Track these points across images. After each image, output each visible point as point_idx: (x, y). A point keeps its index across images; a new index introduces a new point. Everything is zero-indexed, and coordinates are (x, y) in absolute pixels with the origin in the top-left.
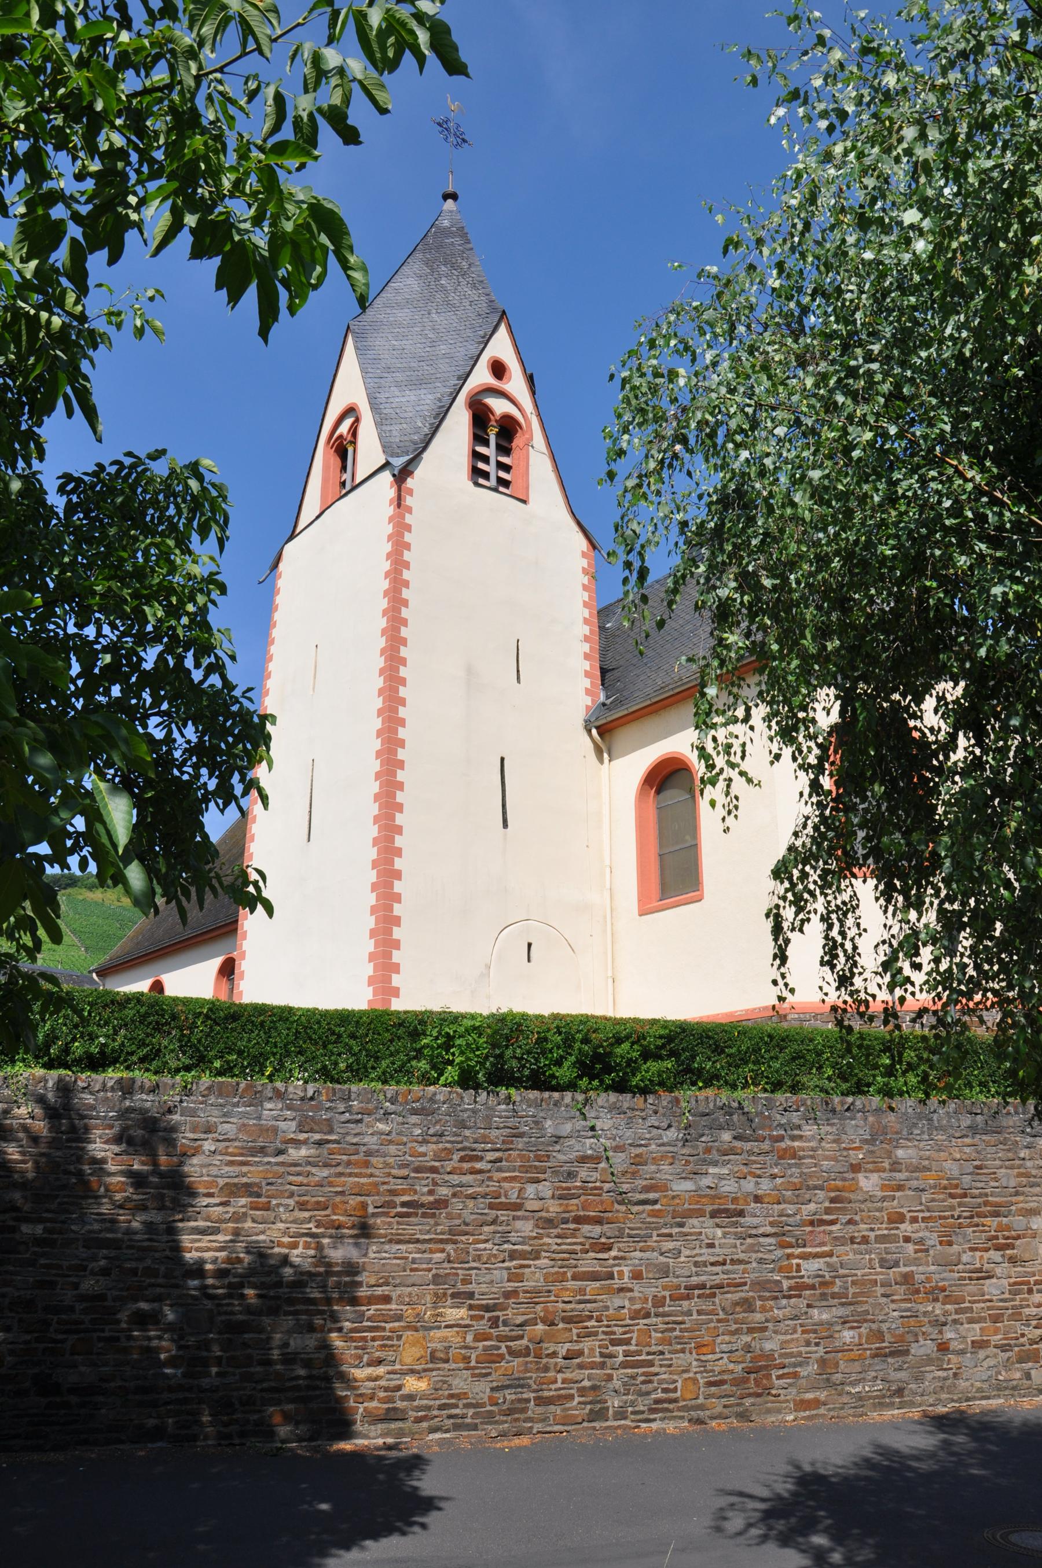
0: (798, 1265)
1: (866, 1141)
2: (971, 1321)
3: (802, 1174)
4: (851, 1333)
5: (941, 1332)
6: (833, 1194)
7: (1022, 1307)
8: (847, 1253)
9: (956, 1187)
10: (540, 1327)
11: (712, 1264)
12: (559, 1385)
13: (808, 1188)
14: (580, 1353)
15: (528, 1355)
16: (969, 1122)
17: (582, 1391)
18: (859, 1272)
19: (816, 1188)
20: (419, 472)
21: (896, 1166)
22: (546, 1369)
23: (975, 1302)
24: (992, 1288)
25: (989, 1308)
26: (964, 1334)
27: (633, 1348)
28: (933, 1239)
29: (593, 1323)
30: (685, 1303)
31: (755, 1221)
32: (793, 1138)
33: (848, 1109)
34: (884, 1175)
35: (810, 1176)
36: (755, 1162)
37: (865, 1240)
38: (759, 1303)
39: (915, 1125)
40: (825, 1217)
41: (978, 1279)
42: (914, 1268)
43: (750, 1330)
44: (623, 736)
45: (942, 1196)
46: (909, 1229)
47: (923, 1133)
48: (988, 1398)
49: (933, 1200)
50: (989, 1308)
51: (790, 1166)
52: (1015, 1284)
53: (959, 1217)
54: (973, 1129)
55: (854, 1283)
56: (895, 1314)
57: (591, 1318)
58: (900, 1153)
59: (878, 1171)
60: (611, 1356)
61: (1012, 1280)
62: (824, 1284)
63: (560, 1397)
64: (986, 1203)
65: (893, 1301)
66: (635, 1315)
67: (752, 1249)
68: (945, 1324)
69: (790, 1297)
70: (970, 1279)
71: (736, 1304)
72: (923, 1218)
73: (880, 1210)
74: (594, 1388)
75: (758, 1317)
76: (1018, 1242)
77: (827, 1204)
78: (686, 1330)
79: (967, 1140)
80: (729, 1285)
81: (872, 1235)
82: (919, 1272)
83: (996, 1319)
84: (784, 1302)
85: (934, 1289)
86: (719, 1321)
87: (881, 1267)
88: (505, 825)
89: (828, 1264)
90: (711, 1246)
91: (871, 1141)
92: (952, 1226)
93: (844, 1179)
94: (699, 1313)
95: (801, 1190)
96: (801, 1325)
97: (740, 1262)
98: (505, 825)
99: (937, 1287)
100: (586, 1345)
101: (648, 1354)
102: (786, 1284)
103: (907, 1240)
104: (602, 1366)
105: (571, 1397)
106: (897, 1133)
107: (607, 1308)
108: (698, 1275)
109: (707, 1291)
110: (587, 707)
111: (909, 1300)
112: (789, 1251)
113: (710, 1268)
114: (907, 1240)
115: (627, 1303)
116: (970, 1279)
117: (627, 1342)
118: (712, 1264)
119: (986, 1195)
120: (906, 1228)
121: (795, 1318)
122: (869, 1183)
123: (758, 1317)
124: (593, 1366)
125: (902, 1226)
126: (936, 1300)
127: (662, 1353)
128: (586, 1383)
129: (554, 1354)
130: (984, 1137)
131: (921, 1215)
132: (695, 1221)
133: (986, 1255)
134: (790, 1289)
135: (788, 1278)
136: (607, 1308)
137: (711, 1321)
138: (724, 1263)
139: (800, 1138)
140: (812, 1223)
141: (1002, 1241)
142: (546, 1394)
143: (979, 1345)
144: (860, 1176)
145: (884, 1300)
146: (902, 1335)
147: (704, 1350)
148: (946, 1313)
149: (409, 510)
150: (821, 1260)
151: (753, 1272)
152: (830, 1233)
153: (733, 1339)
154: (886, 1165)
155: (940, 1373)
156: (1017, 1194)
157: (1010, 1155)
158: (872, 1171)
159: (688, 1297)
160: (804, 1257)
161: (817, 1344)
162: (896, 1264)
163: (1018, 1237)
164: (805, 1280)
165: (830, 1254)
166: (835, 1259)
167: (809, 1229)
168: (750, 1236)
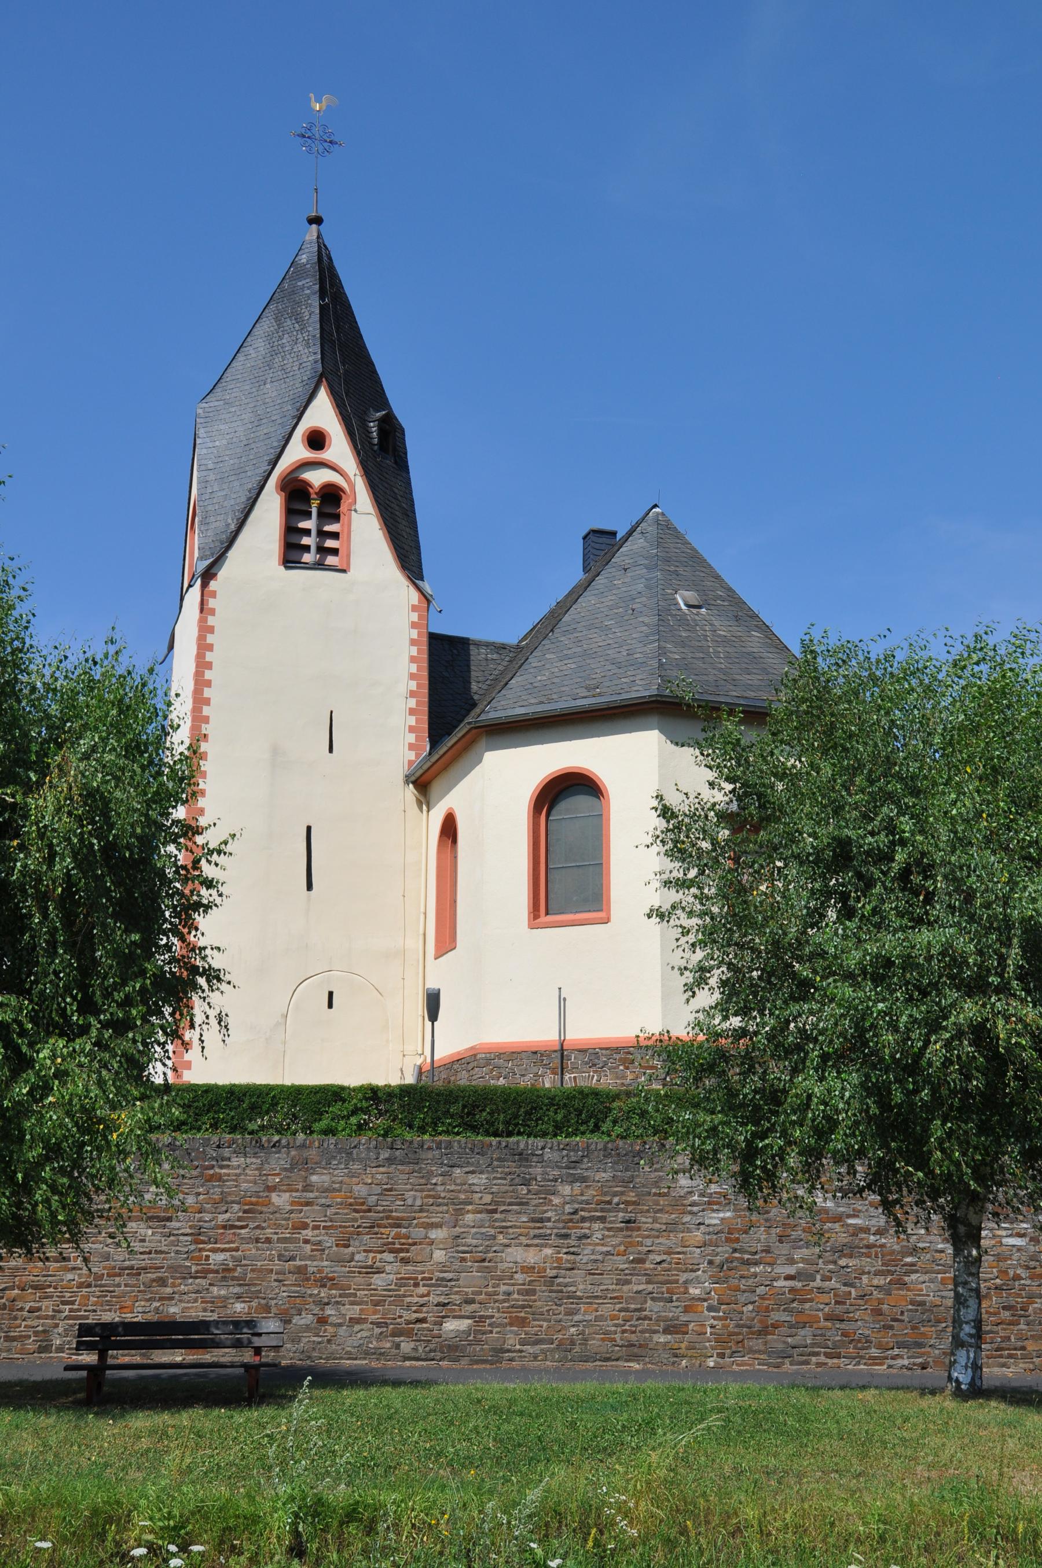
0: (208, 1257)
1: (285, 1169)
2: (352, 1303)
3: (222, 1193)
4: (242, 1305)
5: (322, 1310)
6: (247, 1207)
7: (404, 1296)
8: (251, 1250)
9: (363, 1204)
10: (16, 1291)
11: (141, 1253)
12: (22, 1329)
13: (227, 1203)
14: (39, 1309)
15: (5, 1309)
16: (387, 1155)
17: (36, 1334)
18: (259, 1264)
19: (233, 1202)
20: (224, 573)
21: (308, 1187)
22: (15, 1318)
23: (359, 1290)
24: (378, 1280)
25: (372, 1295)
26: (343, 1312)
27: (75, 1307)
28: (329, 1241)
29: (52, 1290)
30: (117, 1279)
31: (178, 1225)
32: (222, 1167)
33: (274, 1146)
34: (294, 1194)
35: (229, 1194)
36: (186, 1184)
37: (268, 1240)
38: (170, 1281)
39: (334, 1158)
40: (237, 1223)
41: (367, 1273)
42: (308, 1263)
43: (161, 1299)
44: (435, 788)
45: (346, 1211)
46: (310, 1234)
47: (341, 1163)
48: (356, 1359)
49: (336, 1214)
50: (372, 1295)
51: (214, 1187)
52: (402, 1279)
53: (358, 1227)
54: (390, 1161)
55: (252, 1270)
56: (285, 1294)
57: (50, 1286)
58: (314, 1178)
59: (291, 1191)
60: (60, 1312)
61: (399, 1276)
62: (229, 1270)
63: (21, 1336)
64: (388, 1218)
65: (284, 1285)
66: (80, 1285)
67: (172, 1244)
68: (328, 1304)
69: (196, 1278)
70: (360, 1273)
71: (154, 1280)
72: (325, 1227)
73: (288, 1219)
74: (44, 1331)
75: (169, 1290)
76: (413, 1248)
77: (240, 1214)
78: (114, 1297)
79: (381, 1169)
80: (151, 1268)
81: (275, 1237)
82: (312, 1266)
83: (376, 1304)
84: (190, 1281)
85: (322, 1278)
86: (139, 1291)
87: (279, 1260)
88: (310, 887)
89: (232, 1257)
90: (143, 1241)
91: (290, 1170)
92: (352, 1233)
93: (259, 1197)
94: (126, 1285)
95: (224, 1201)
96: (202, 1298)
97: (161, 1252)
98: (310, 887)
99: (326, 1277)
100: (45, 1304)
101: (85, 1311)
102: (194, 1269)
103: (306, 1242)
104: (53, 1317)
105: (30, 1337)
106: (316, 1163)
107: (63, 1280)
108: (129, 1259)
109: (136, 1272)
110: (410, 763)
111: (300, 1286)
112: (201, 1246)
113: (139, 1256)
114: (306, 1242)
115: (76, 1278)
116: (360, 1273)
117: (73, 1303)
118: (141, 1253)
119: (391, 1211)
120: (308, 1233)
121: (197, 1292)
122: (280, 1200)
123: (169, 1290)
124: (46, 1317)
125: (304, 1232)
126: (324, 1286)
127: (95, 1311)
128: (40, 1328)
129: (22, 1309)
130: (399, 1167)
131: (323, 1224)
132: (134, 1224)
133: (379, 1256)
134: (197, 1272)
135: (197, 1264)
136: (63, 1280)
137: (133, 1291)
138: (150, 1253)
139: (228, 1166)
140: (224, 1227)
141: (397, 1246)
142: (12, 1334)
143: (354, 1321)
144: (274, 1195)
145: (276, 1284)
146: (287, 1309)
147: (125, 1310)
148: (329, 1296)
149: (212, 612)
150: (228, 1254)
151: (172, 1258)
152: (240, 1234)
153: (148, 1304)
154: (300, 1187)
155: (315, 1339)
156: (421, 1211)
157: (423, 1181)
158: (285, 1191)
159: (119, 1275)
160: (214, 1251)
161: (212, 1311)
162: (292, 1258)
163: (415, 1244)
164: (212, 1267)
165: (237, 1250)
166: (240, 1253)
167: (222, 1231)
168: (174, 1235)
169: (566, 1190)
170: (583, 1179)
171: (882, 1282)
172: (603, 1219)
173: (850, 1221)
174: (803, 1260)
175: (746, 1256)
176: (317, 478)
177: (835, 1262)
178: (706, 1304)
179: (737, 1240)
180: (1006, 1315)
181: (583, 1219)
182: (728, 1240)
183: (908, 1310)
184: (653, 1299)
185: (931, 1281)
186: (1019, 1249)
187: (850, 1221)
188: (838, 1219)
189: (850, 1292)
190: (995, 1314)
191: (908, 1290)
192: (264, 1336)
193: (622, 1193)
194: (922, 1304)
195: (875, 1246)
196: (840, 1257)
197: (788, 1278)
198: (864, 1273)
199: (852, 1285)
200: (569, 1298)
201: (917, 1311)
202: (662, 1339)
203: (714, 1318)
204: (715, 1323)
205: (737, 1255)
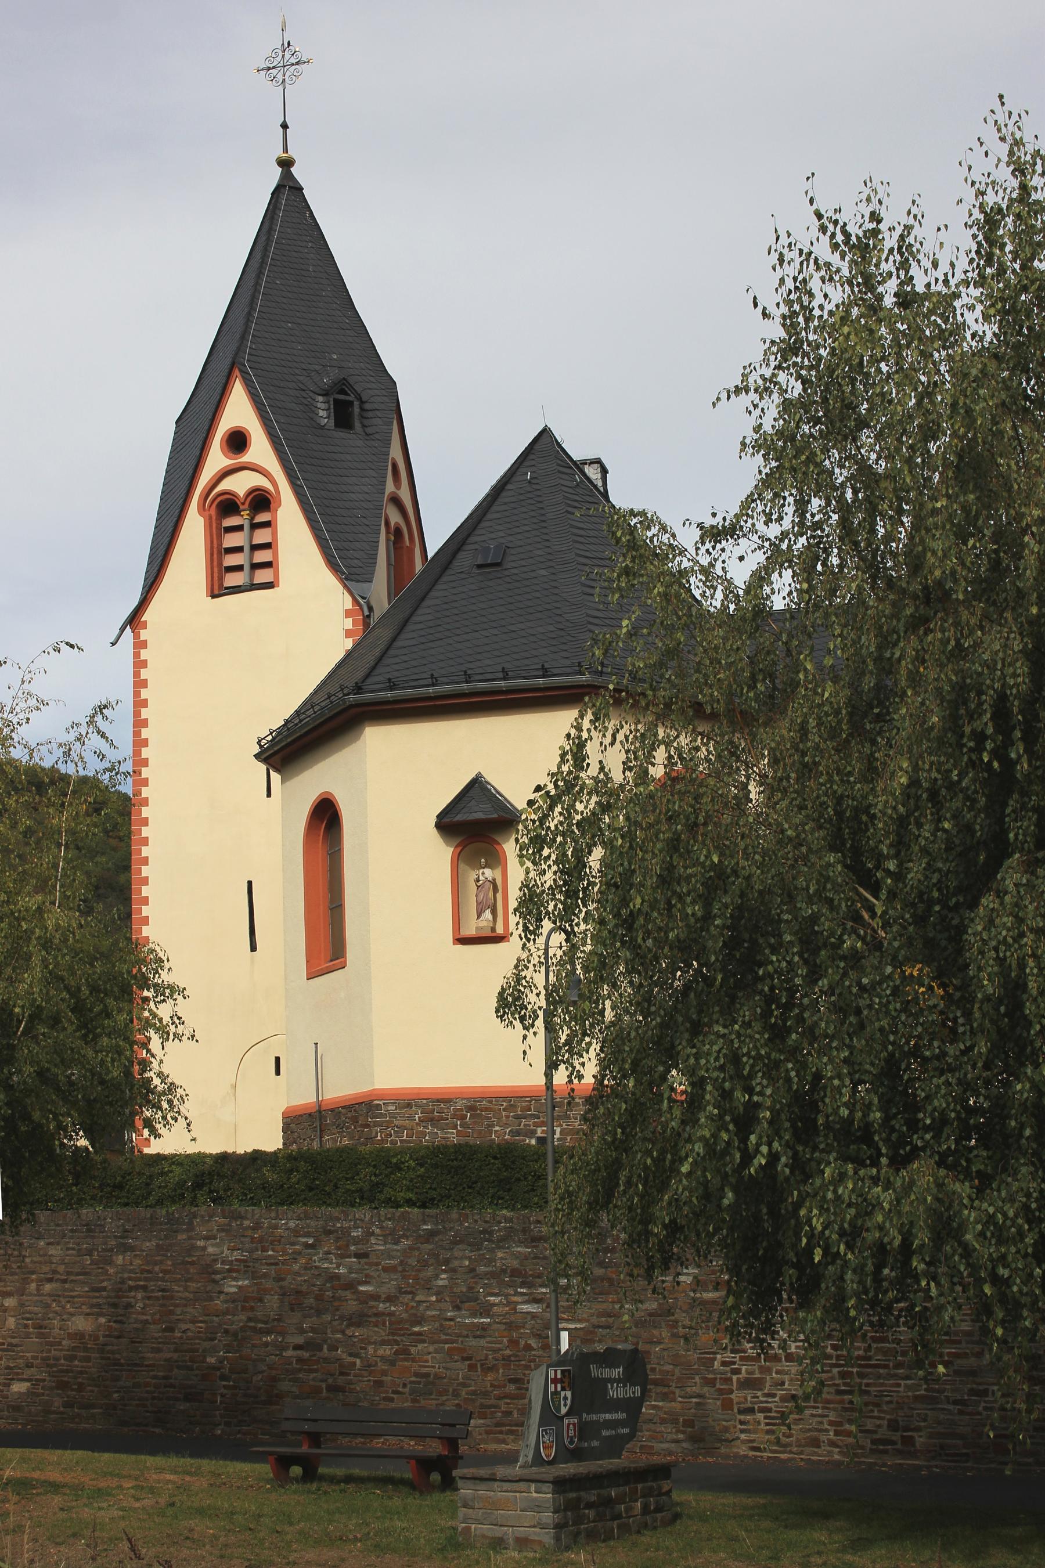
98: (253, 948)
169: (119, 1260)
170: (132, 1249)
171: (388, 1352)
172: (144, 1288)
173: (362, 1288)
174: (313, 1330)
175: (260, 1325)
176: (240, 485)
177: (343, 1332)
178: (218, 1373)
179: (252, 1309)
180: (511, 1388)
181: (131, 1288)
182: (244, 1308)
183: (411, 1382)
184: (178, 1367)
185: (436, 1351)
186: (534, 1316)
187: (362, 1288)
188: (351, 1286)
189: (354, 1364)
190: (499, 1387)
191: (414, 1360)
192: (550, 1478)
193: (161, 1262)
194: (427, 1375)
195: (383, 1314)
196: (348, 1326)
197: (297, 1347)
198: (370, 1343)
199: (356, 1355)
200: (115, 1365)
201: (419, 1383)
202: (182, 1406)
203: (225, 1387)
204: (225, 1392)
205: (252, 1324)
